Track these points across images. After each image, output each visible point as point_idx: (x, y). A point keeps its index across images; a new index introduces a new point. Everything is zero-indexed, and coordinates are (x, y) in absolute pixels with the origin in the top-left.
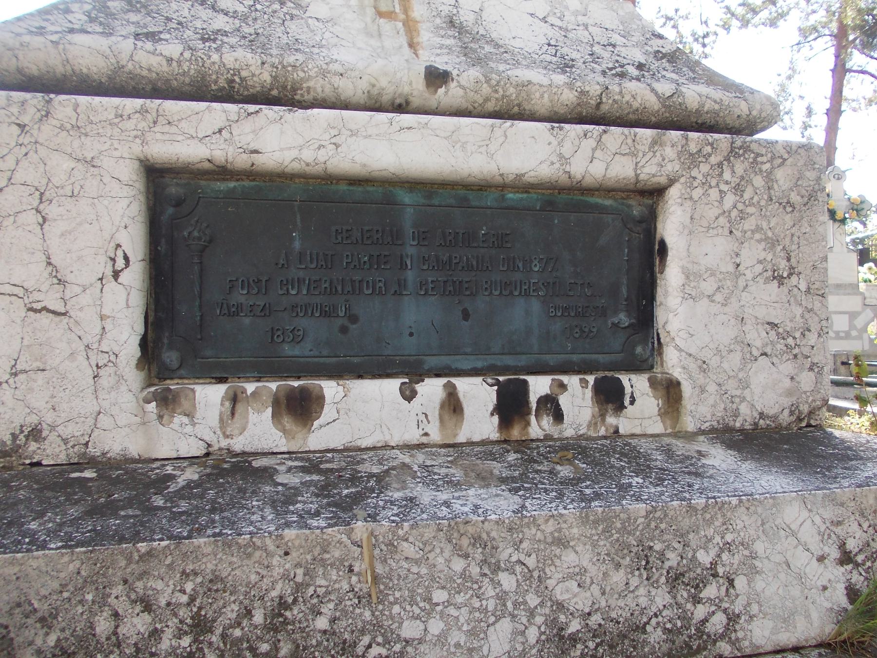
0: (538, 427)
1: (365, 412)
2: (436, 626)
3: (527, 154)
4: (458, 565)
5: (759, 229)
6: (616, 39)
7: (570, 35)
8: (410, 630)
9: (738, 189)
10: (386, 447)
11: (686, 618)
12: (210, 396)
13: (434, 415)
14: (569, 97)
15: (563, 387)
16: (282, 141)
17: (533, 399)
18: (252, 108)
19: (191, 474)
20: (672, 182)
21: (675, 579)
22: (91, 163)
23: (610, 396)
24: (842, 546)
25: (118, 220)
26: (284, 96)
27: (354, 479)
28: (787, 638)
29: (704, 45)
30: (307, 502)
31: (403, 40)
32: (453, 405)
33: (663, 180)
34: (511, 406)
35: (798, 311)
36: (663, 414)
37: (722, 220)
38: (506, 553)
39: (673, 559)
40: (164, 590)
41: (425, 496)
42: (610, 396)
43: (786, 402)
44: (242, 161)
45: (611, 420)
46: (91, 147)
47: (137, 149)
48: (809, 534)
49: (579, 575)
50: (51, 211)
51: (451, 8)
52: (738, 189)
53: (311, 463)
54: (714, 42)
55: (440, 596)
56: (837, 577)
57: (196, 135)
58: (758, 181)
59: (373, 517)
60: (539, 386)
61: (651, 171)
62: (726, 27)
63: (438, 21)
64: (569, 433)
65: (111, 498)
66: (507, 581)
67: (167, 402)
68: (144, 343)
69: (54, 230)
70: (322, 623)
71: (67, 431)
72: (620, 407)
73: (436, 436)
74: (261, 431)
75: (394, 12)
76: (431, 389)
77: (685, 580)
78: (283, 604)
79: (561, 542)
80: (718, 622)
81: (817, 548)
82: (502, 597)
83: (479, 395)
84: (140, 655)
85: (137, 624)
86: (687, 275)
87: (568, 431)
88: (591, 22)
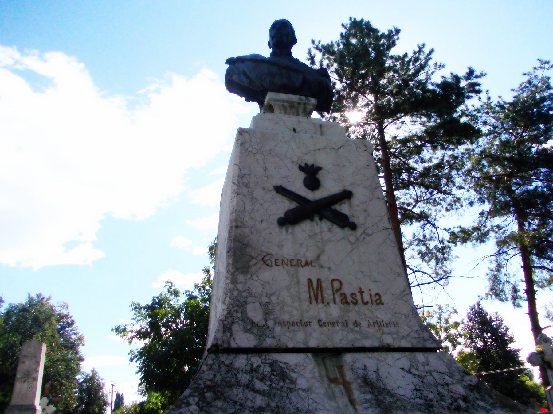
6: (448, 379)
7: (425, 381)
29: (443, 254)
31: (346, 400)
51: (363, 371)
54: (449, 252)
62: (454, 242)
63: (359, 381)
75: (336, 378)
88: (432, 369)
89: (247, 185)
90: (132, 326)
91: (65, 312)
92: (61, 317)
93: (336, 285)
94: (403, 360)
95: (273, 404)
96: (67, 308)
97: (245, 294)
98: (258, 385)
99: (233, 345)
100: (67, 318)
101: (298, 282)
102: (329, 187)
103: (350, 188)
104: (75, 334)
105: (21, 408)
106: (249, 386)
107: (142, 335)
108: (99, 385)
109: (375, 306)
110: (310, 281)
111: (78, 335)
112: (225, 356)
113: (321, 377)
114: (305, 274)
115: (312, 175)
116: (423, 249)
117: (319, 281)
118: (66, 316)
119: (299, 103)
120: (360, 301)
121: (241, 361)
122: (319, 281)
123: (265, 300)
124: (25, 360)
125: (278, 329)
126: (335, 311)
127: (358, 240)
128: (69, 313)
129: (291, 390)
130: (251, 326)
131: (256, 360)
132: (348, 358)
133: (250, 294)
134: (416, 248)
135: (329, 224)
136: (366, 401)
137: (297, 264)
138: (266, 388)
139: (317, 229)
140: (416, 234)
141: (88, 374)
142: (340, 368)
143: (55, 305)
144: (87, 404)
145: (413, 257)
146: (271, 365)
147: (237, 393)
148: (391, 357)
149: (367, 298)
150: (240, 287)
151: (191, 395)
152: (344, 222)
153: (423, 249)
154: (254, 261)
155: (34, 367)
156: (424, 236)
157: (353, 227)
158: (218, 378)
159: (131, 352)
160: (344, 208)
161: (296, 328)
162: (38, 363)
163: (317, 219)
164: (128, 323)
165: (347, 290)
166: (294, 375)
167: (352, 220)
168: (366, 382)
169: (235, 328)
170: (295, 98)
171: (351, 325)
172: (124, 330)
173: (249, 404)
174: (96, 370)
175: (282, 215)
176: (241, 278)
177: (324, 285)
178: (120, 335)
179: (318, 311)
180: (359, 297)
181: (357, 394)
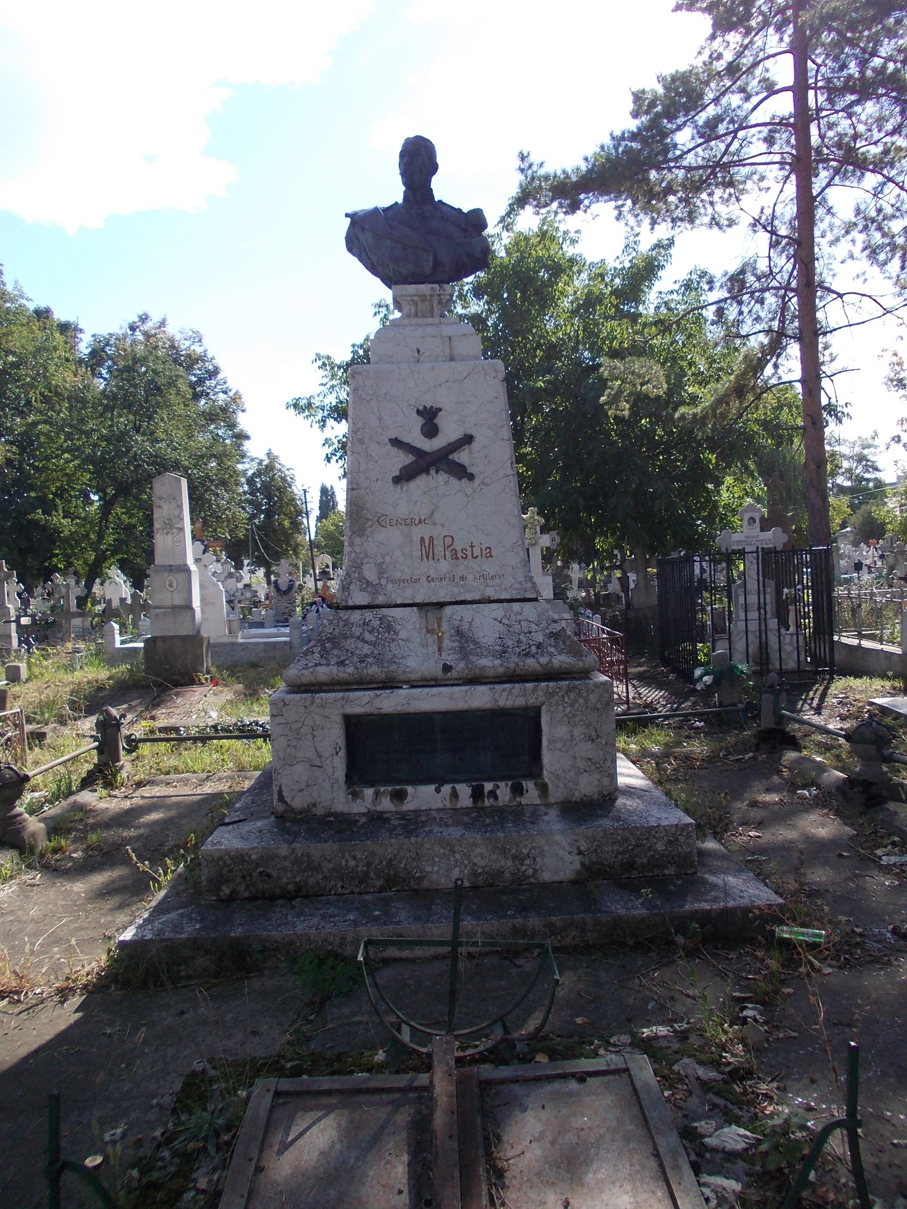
0: (488, 802)
1: (424, 797)
2: (436, 868)
3: (480, 698)
4: (442, 851)
5: (582, 720)
8: (428, 869)
9: (572, 705)
10: (430, 810)
11: (519, 870)
12: (369, 792)
13: (448, 798)
14: (501, 670)
15: (498, 787)
16: (391, 702)
17: (486, 792)
18: (379, 692)
19: (364, 820)
20: (543, 704)
21: (514, 857)
22: (327, 717)
23: (517, 790)
24: (578, 849)
25: (336, 734)
26: (389, 684)
27: (416, 823)
28: (556, 878)
30: (399, 830)
32: (454, 795)
33: (538, 704)
34: (477, 794)
35: (601, 753)
36: (540, 796)
37: (565, 719)
38: (457, 848)
39: (513, 851)
40: (359, 854)
41: (436, 829)
42: (517, 790)
43: (596, 790)
44: (376, 712)
45: (518, 799)
46: (327, 712)
47: (341, 711)
48: (564, 844)
49: (482, 856)
50: (316, 733)
52: (572, 705)
53: (403, 816)
55: (437, 860)
56: (577, 859)
57: (362, 702)
58: (581, 701)
59: (417, 836)
60: (488, 786)
61: (532, 701)
64: (501, 804)
65: (339, 826)
66: (458, 856)
67: (355, 795)
68: (346, 775)
69: (317, 739)
70: (402, 866)
71: (323, 804)
72: (522, 794)
73: (448, 805)
74: (386, 804)
76: (447, 789)
77: (518, 858)
78: (391, 860)
79: (475, 845)
80: (530, 872)
81: (568, 849)
82: (456, 861)
83: (464, 790)
84: (900, 241)
85: (352, 863)
86: (549, 742)
87: (500, 803)
89: (361, 441)
90: (321, 398)
91: (198, 349)
92: (192, 361)
93: (448, 541)
94: (497, 610)
95: (376, 652)
96: (200, 341)
97: (361, 556)
98: (368, 636)
99: (351, 603)
100: (204, 361)
101: (411, 541)
102: (449, 432)
103: (469, 432)
104: (225, 392)
105: (171, 569)
106: (360, 638)
107: (339, 412)
108: (284, 479)
109: (484, 559)
110: (422, 539)
111: (231, 394)
112: (343, 612)
113: (421, 628)
114: (418, 532)
115: (430, 419)
116: (877, 238)
117: (431, 539)
118: (201, 358)
119: (431, 296)
120: (470, 556)
121: (356, 616)
122: (431, 539)
123: (379, 560)
124: (161, 503)
125: (390, 586)
126: (444, 566)
127: (475, 491)
128: (205, 351)
129: (393, 640)
130: (367, 585)
131: (368, 615)
132: (448, 610)
133: (366, 555)
134: (860, 238)
135: (446, 476)
136: (453, 648)
137: (409, 522)
138: (373, 639)
139: (433, 484)
140: (862, 207)
141: (262, 461)
142: (439, 620)
143: (178, 337)
144: (269, 514)
145: (852, 257)
146: (381, 619)
147: (350, 643)
148: (487, 608)
149: (477, 552)
150: (357, 549)
151: (315, 646)
152: (461, 472)
153: (877, 238)
154: (370, 523)
155: (176, 513)
156: (879, 211)
157: (471, 477)
158: (337, 632)
159: (327, 442)
160: (461, 457)
161: (406, 584)
162: (180, 507)
163: (433, 472)
164: (314, 393)
165: (458, 546)
166: (398, 627)
167: (470, 470)
168: (459, 632)
169: (352, 587)
170: (425, 288)
171: (457, 580)
172: (309, 405)
173: (358, 652)
174: (275, 452)
175: (397, 473)
176: (358, 540)
177: (436, 542)
178: (302, 415)
179: (429, 568)
180: (469, 553)
181: (446, 643)
